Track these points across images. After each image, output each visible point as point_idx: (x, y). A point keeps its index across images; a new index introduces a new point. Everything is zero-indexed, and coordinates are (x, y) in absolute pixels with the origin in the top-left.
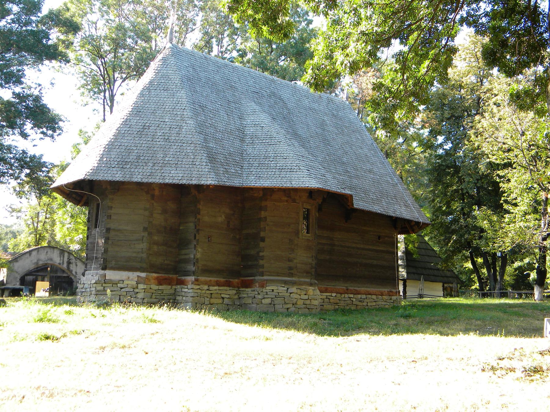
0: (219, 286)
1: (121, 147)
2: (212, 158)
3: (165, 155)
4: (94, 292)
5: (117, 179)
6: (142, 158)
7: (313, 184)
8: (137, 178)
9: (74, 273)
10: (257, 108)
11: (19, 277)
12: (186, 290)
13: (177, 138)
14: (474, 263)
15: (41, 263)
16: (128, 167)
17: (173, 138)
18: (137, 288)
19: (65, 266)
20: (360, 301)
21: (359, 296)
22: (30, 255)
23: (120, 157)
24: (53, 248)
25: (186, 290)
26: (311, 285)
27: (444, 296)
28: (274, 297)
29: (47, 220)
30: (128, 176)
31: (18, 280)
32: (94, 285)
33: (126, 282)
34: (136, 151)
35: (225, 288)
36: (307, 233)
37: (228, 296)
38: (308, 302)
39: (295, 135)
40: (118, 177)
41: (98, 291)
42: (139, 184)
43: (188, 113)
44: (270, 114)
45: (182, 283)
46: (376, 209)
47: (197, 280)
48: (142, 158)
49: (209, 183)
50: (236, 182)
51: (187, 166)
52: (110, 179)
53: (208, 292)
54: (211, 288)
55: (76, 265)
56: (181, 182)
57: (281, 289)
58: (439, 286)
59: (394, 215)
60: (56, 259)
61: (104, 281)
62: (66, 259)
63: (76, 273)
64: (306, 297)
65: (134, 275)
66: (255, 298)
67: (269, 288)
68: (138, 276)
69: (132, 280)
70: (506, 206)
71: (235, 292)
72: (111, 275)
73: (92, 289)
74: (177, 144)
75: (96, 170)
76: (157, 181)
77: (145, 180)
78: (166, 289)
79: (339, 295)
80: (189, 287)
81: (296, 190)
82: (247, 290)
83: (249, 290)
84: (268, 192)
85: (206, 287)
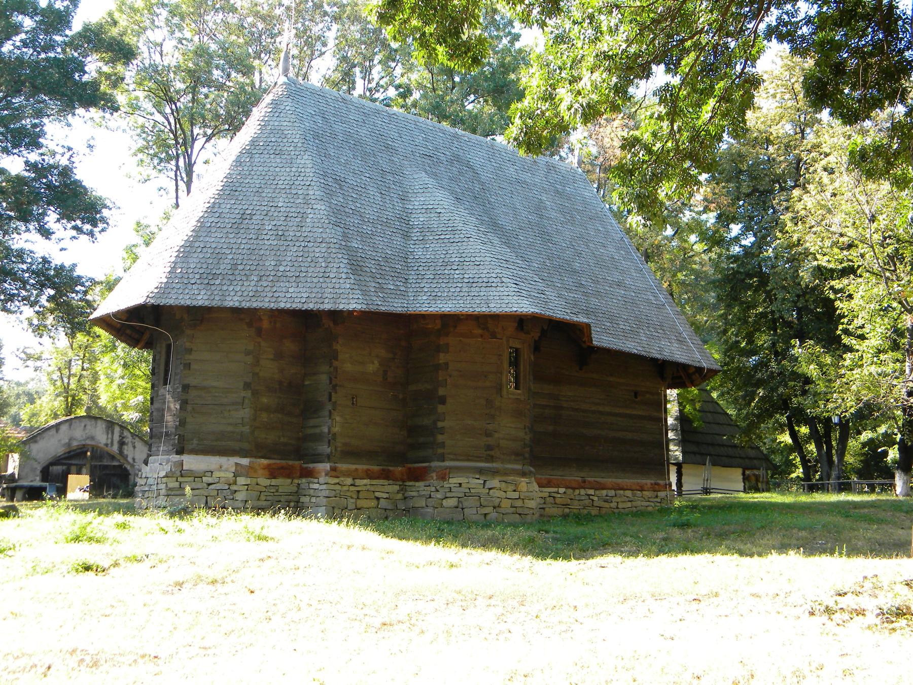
1: (205, 250)
2: (356, 267)
4: (163, 492)
5: (200, 303)
6: (240, 267)
7: (525, 306)
12: (316, 486)
13: (298, 234)
14: (794, 435)
15: (75, 444)
16: (218, 282)
18: (235, 483)
19: (115, 447)
20: (606, 501)
21: (604, 492)
24: (96, 418)
25: (316, 486)
26: (524, 474)
27: (745, 491)
29: (84, 373)
30: (217, 298)
31: (38, 472)
32: (164, 480)
33: (217, 474)
34: (230, 257)
35: (381, 482)
36: (517, 388)
37: (385, 496)
38: (519, 503)
40: (201, 299)
41: (170, 489)
43: (315, 192)
45: (309, 474)
46: (631, 346)
47: (334, 469)
48: (240, 267)
49: (351, 307)
50: (397, 306)
51: (315, 280)
52: (188, 303)
53: (352, 488)
54: (358, 482)
55: (134, 447)
56: (305, 307)
57: (474, 483)
58: (737, 474)
59: (659, 356)
60: (101, 436)
61: (180, 473)
62: (116, 438)
63: (134, 459)
64: (516, 495)
65: (229, 463)
66: (430, 497)
68: (236, 464)
69: (226, 470)
70: (846, 340)
71: (397, 488)
72: (192, 462)
74: (298, 244)
75: (164, 289)
76: (266, 305)
79: (570, 491)
80: (322, 480)
82: (417, 484)
84: (450, 321)
85: (349, 481)
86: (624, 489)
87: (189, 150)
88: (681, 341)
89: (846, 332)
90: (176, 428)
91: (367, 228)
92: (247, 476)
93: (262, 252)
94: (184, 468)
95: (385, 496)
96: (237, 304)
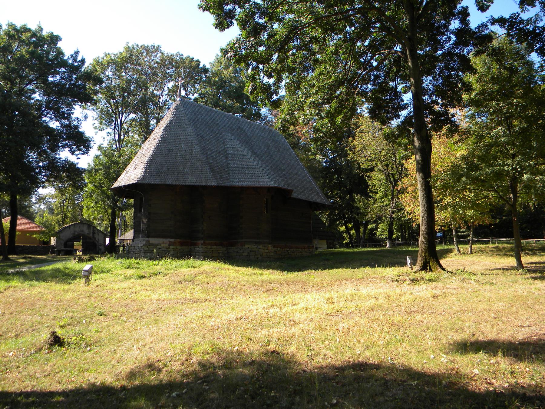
0: (216, 246)
1: (157, 163)
2: (212, 170)
3: (184, 168)
4: (143, 251)
5: (157, 183)
6: (170, 169)
7: (272, 184)
8: (169, 182)
9: (97, 239)
10: (232, 136)
11: (63, 242)
12: (198, 249)
13: (190, 157)
14: (347, 227)
15: (76, 233)
16: (163, 175)
17: (188, 157)
18: (169, 248)
19: (91, 235)
20: (293, 253)
21: (292, 250)
22: (69, 228)
23: (157, 169)
24: (84, 224)
25: (198, 249)
26: (270, 244)
27: (328, 248)
28: (249, 251)
29: (69, 205)
30: (163, 181)
31: (63, 244)
32: (143, 247)
33: (162, 245)
34: (166, 166)
35: (220, 247)
36: (267, 212)
37: (221, 252)
38: (268, 254)
39: (254, 152)
40: (157, 181)
41: (145, 250)
42: (169, 185)
43: (195, 142)
44: (240, 141)
45: (195, 245)
46: (302, 197)
47: (204, 243)
48: (170, 169)
49: (213, 184)
50: (228, 184)
51: (198, 174)
52: (153, 183)
53: (211, 249)
54: (213, 247)
55: (98, 234)
56: (196, 184)
57: (254, 247)
58: (325, 242)
59: (312, 201)
60: (86, 230)
61: (148, 244)
62: (92, 231)
63: (98, 239)
64: (267, 251)
65: (167, 241)
66: (238, 252)
67: (246, 246)
68: (169, 241)
69: (166, 243)
70: (371, 194)
71: (225, 249)
72: (152, 241)
73: (141, 249)
74: (191, 161)
75: (143, 177)
76: (182, 183)
77: (174, 183)
78: (185, 248)
79: (281, 249)
80: (200, 246)
81: (261, 188)
82: (233, 248)
83: (234, 247)
84: (243, 189)
85: (209, 247)
86: (299, 248)
87: (121, 116)
88: (318, 195)
89: (370, 191)
90: (146, 228)
91: (214, 155)
92: (173, 246)
93: (178, 164)
94: (150, 242)
95: (221, 252)
96: (171, 183)
